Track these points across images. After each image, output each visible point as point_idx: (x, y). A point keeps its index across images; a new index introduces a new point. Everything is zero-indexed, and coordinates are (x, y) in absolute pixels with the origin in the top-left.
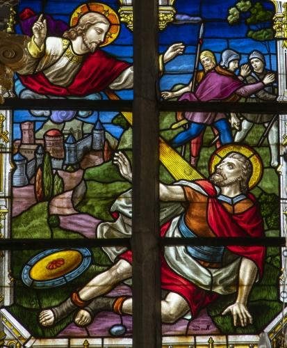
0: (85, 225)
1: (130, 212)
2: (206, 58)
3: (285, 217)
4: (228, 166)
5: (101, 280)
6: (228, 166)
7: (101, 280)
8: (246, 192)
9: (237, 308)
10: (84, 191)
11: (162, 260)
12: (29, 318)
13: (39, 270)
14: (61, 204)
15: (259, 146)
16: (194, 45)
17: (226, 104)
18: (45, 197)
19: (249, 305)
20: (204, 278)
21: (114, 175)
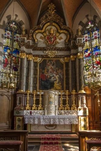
0: (89, 64)
1: (4, 22)
2: (96, 52)
3: (71, 62)
4: (98, 59)
5: (90, 68)
6: (98, 59)
7: (90, 68)
8: (99, 60)
9: (99, 68)
10: (12, 109)
11: (94, 66)
12: (86, 71)
13: (87, 68)
14: (88, 63)
15: (100, 57)
16: (95, 51)
17: (97, 55)
18: (87, 63)
19: (100, 68)
20: (97, 66)
21: (91, 61)
